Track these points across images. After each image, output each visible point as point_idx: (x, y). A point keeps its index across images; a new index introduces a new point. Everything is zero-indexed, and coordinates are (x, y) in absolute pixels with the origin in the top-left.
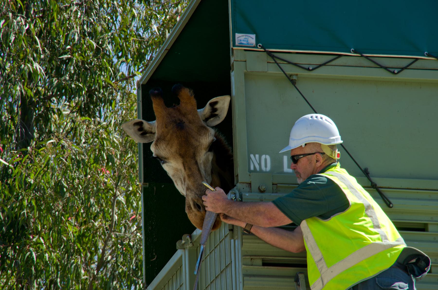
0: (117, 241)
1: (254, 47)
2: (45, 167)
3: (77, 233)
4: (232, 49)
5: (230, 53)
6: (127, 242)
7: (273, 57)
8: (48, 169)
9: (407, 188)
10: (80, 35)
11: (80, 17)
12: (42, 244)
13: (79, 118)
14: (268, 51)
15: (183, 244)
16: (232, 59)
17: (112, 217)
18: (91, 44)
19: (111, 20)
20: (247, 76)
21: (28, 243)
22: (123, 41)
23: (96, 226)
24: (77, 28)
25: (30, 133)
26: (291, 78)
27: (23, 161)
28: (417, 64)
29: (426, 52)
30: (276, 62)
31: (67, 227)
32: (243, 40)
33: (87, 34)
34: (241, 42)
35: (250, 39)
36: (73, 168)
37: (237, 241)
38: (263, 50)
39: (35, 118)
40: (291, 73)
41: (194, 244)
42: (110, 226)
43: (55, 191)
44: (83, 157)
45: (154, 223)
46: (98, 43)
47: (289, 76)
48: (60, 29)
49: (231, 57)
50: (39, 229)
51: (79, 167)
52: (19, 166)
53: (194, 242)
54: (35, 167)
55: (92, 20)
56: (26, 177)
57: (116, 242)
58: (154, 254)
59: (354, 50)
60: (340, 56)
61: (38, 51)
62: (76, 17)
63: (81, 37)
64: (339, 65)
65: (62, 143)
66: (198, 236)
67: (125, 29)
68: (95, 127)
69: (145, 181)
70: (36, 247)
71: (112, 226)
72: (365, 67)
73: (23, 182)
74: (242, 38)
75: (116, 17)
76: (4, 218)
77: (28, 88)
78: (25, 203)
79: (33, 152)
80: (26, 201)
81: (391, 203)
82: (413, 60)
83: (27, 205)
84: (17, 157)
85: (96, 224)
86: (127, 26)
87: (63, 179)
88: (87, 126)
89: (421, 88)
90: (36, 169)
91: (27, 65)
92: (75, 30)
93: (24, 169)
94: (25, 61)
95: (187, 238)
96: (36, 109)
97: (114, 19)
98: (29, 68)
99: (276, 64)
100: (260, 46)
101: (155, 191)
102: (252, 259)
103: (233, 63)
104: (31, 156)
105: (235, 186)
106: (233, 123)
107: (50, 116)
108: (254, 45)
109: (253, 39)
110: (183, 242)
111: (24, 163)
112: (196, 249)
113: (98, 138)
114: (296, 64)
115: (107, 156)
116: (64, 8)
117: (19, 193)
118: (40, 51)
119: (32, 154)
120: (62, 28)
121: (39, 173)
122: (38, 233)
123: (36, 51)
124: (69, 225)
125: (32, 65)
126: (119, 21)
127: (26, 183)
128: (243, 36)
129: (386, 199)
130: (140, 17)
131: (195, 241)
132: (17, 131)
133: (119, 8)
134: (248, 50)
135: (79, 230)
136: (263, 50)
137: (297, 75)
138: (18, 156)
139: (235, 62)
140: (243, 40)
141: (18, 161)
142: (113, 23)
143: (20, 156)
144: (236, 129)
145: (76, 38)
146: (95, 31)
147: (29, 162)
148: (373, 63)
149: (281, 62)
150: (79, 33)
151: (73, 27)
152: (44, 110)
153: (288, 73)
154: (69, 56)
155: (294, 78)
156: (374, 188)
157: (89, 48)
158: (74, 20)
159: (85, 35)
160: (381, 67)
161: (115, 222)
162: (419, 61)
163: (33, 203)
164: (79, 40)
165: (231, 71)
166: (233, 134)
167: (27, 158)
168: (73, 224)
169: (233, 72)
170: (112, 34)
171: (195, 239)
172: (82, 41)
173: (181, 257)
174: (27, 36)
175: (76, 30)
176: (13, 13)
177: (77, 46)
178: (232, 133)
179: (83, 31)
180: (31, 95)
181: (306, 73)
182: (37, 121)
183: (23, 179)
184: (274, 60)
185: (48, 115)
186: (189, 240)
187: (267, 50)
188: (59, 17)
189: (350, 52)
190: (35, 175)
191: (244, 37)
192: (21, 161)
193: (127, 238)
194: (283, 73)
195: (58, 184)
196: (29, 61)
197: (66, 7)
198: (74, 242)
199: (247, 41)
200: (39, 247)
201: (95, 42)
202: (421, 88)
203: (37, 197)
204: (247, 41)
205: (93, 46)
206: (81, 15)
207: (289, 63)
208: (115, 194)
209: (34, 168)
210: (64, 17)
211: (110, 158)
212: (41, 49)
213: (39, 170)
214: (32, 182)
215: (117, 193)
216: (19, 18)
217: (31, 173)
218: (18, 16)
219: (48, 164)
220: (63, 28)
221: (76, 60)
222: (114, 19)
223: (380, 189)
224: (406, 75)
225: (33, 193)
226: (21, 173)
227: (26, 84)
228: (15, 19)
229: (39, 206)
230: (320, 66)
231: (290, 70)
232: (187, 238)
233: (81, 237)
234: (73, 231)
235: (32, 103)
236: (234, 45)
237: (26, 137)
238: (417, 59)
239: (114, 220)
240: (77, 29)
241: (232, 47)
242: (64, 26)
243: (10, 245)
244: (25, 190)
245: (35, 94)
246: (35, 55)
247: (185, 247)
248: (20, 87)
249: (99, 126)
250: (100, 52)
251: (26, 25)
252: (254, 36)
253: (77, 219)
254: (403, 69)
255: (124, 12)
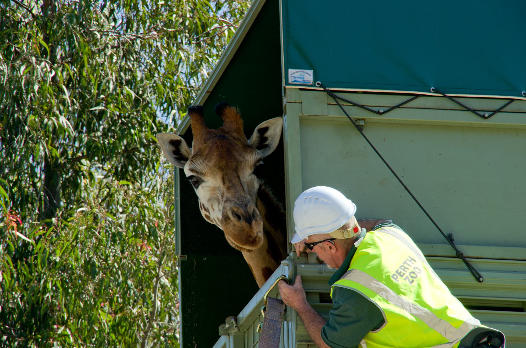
0: (160, 332)
1: (311, 86)
2: (73, 241)
3: (112, 321)
4: (284, 87)
5: (282, 93)
6: (173, 334)
7: (335, 97)
8: (77, 243)
9: (500, 257)
10: (115, 83)
11: (116, 63)
12: (68, 336)
13: (116, 182)
14: (328, 90)
15: (227, 329)
16: (285, 100)
17: (154, 303)
18: (129, 94)
19: (154, 66)
20: (303, 121)
21: (52, 335)
22: (168, 90)
23: (134, 314)
24: (112, 74)
25: (55, 201)
26: (357, 124)
27: (47, 234)
28: (512, 107)
29: (523, 92)
30: (338, 104)
31: (99, 315)
32: (298, 78)
33: (124, 82)
34: (295, 79)
35: (306, 75)
36: (107, 244)
37: (290, 323)
38: (322, 89)
39: (62, 184)
40: (357, 117)
41: (240, 328)
42: (152, 313)
43: (86, 271)
44: (120, 230)
45: (194, 304)
46: (137, 93)
47: (354, 121)
48: (91, 76)
49: (283, 98)
50: (66, 318)
51: (114, 241)
52: (42, 241)
53: (240, 326)
54: (62, 242)
55: (131, 66)
56: (50, 254)
57: (158, 333)
58: (194, 342)
59: (434, 88)
60: (417, 96)
61: (66, 103)
62: (111, 62)
63: (117, 85)
64: (416, 107)
65: (94, 212)
66: (245, 319)
67: (170, 76)
68: (135, 193)
69: (183, 253)
70: (62, 341)
71: (154, 314)
72: (448, 110)
73: (46, 260)
74: (297, 75)
75: (161, 61)
76: (25, 306)
77: (52, 146)
78: (49, 286)
79: (60, 223)
80: (50, 283)
81: (480, 277)
82: (507, 101)
83: (52, 289)
84: (40, 230)
85: (135, 311)
86: (173, 73)
87: (95, 257)
88: (126, 192)
89: (517, 135)
90: (63, 244)
91: (52, 120)
92: (110, 77)
93: (48, 244)
94: (49, 114)
95: (231, 321)
96: (63, 173)
97: (158, 64)
98: (54, 124)
99: (338, 106)
100: (318, 84)
101: (195, 265)
102: (308, 345)
103: (286, 105)
104: (56, 228)
105: (289, 255)
106: (285, 179)
107: (79, 181)
108: (311, 83)
109: (310, 75)
110: (227, 326)
111: (48, 237)
112: (243, 334)
113: (138, 207)
114: (362, 107)
115: (148, 228)
116: (97, 51)
117: (41, 273)
118: (68, 102)
119: (58, 226)
120: (93, 75)
121: (67, 248)
122: (64, 323)
123: (63, 102)
124: (102, 312)
125: (57, 118)
126: (164, 67)
127: (50, 262)
128: (298, 72)
129: (476, 274)
130: (188, 61)
131: (242, 325)
132: (40, 200)
133: (163, 50)
134: (304, 89)
135: (114, 319)
136: (322, 89)
137: (364, 119)
138: (41, 228)
139: (288, 104)
140: (298, 78)
141: (41, 234)
142: (156, 68)
143: (43, 228)
144: (289, 185)
145: (111, 86)
146: (134, 77)
147: (54, 235)
148: (457, 104)
149: (345, 104)
150: (114, 81)
151: (108, 74)
152: (72, 174)
153: (354, 116)
154: (103, 108)
155: (361, 123)
156: (460, 259)
157: (126, 99)
158: (109, 65)
159: (121, 83)
160: (468, 110)
161: (158, 308)
162: (515, 102)
163: (59, 285)
164: (115, 89)
165: (283, 115)
166: (286, 192)
167: (52, 231)
168: (107, 312)
169: (286, 116)
170: (155, 82)
171: (241, 322)
172: (118, 90)
173: (225, 345)
174: (53, 85)
175: (111, 77)
176: (36, 57)
177: (112, 97)
178: (285, 191)
179: (120, 78)
180: (56, 155)
181: (376, 117)
182: (64, 187)
183: (47, 257)
184: (336, 102)
185: (77, 179)
186: (234, 323)
187: (327, 88)
188: (91, 62)
189: (430, 92)
190: (61, 251)
191: (300, 73)
192: (44, 234)
193: (172, 328)
194: (347, 117)
195: (88, 262)
196: (54, 115)
197: (99, 50)
198: (108, 334)
199: (303, 78)
200: (65, 341)
201: (135, 92)
202: (517, 135)
203: (63, 278)
204: (303, 78)
205: (132, 96)
206: (117, 60)
207: (355, 105)
208: (158, 274)
209: (60, 243)
210: (97, 62)
211: (153, 233)
212: (69, 101)
213: (67, 244)
214: (58, 260)
215: (160, 273)
216: (43, 64)
217: (56, 249)
218: (41, 61)
219: (76, 238)
220: (95, 75)
221: (110, 113)
222: (158, 64)
223: (468, 259)
224: (499, 119)
225: (59, 273)
226: (45, 249)
227: (50, 142)
228: (40, 65)
229: (65, 290)
230: (393, 108)
231: (356, 113)
232: (231, 321)
233: (115, 328)
234: (106, 319)
235: (57, 166)
236: (287, 83)
237: (50, 206)
238: (512, 100)
239: (157, 307)
240: (112, 76)
241: (284, 85)
242: (97, 72)
243: (31, 338)
244: (50, 270)
245: (62, 154)
246: (62, 108)
247: (229, 332)
248: (43, 146)
249: (140, 192)
250: (140, 103)
251: (51, 72)
252: (311, 72)
253: (111, 305)
254: (495, 112)
255: (168, 55)
